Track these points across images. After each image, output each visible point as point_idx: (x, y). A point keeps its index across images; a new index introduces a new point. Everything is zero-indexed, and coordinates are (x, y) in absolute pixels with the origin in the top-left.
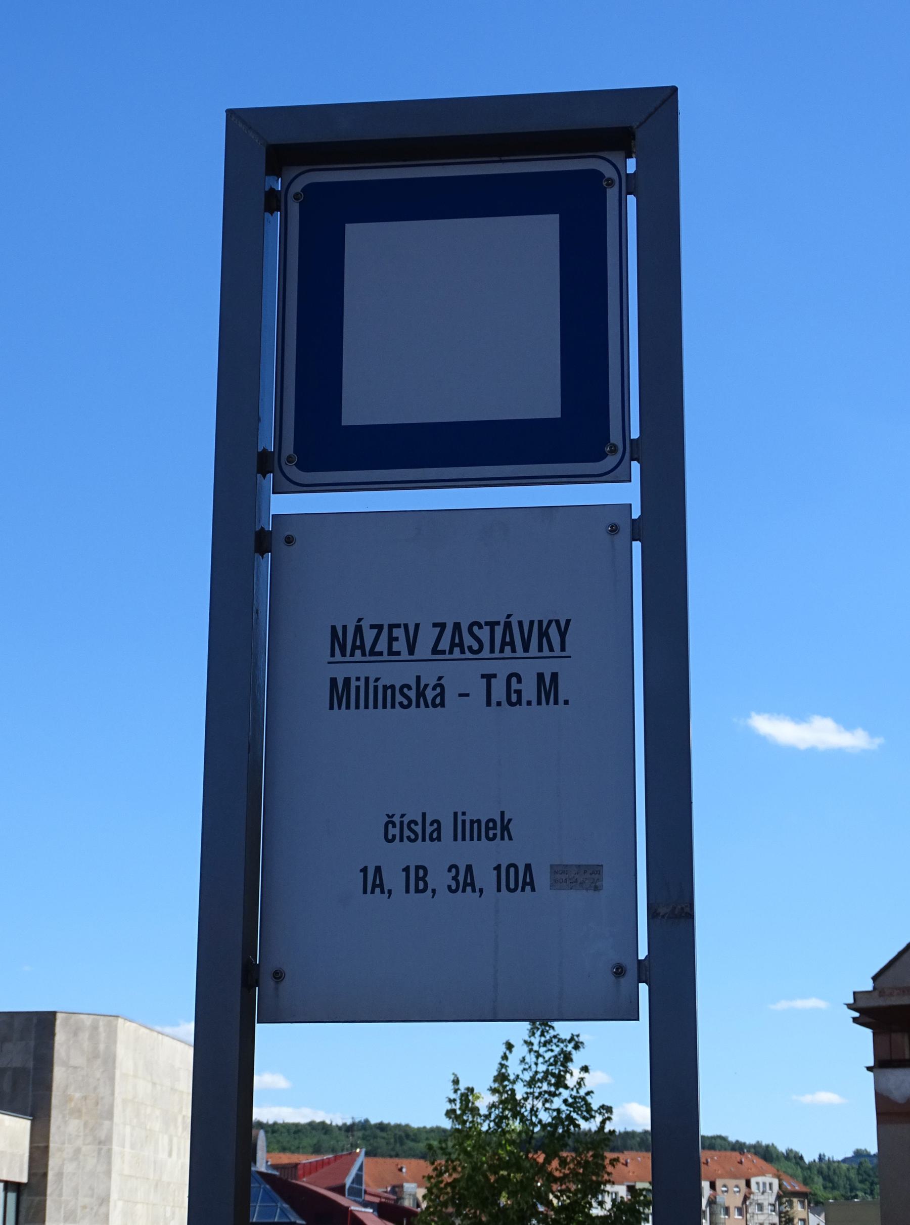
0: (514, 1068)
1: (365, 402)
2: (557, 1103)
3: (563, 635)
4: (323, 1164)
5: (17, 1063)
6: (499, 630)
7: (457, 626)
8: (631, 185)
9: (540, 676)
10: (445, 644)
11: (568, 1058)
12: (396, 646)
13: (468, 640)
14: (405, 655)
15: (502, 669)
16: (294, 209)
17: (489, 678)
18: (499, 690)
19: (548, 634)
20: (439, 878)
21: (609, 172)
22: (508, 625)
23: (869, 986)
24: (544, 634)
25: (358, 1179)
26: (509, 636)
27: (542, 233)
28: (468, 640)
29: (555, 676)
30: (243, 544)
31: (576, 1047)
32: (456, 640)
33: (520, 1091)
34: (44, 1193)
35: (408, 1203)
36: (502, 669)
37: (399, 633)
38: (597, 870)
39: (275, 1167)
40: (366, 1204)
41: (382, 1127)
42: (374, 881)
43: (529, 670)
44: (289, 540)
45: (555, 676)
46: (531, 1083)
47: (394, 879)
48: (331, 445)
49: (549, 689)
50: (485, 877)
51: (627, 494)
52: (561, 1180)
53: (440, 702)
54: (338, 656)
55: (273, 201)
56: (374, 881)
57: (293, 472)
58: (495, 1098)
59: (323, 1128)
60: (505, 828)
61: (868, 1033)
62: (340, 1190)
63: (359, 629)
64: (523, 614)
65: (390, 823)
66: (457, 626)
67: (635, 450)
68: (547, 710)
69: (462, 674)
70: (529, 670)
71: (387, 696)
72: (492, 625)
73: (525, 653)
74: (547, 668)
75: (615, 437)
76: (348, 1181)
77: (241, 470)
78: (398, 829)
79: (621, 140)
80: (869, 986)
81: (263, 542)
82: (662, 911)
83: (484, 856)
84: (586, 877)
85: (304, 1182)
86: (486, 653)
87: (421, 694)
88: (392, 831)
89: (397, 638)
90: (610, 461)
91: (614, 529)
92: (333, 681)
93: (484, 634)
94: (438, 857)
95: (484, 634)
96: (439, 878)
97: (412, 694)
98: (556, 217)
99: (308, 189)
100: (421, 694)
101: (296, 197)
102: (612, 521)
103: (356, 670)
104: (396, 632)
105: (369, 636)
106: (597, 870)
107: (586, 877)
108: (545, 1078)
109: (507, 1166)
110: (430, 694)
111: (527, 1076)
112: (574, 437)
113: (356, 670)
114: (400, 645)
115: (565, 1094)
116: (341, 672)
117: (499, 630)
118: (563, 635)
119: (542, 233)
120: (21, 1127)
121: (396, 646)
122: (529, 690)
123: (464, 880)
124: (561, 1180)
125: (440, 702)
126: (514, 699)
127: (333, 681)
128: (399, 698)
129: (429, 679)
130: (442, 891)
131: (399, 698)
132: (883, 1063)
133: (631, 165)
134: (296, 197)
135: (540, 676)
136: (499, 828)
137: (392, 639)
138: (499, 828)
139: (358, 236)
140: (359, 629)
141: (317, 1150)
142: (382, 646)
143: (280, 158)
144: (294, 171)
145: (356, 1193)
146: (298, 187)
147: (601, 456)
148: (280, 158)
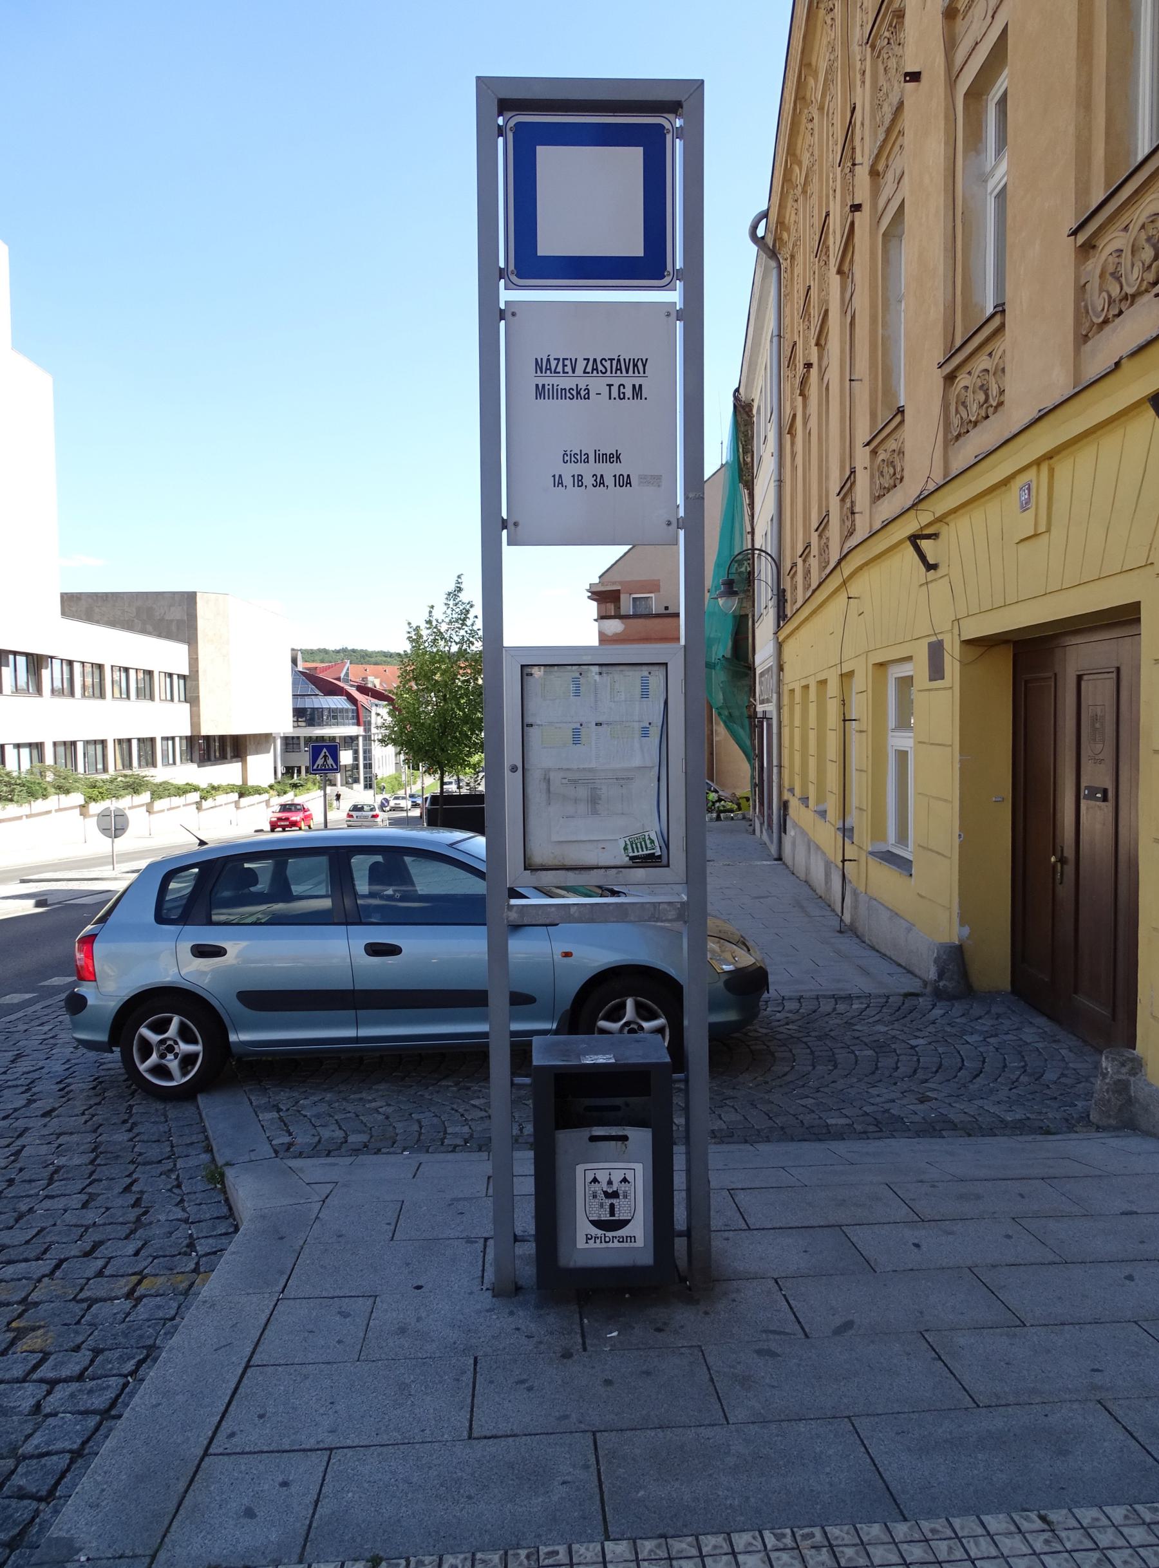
0: (438, 614)
1: (549, 245)
2: (462, 632)
3: (644, 366)
4: (329, 667)
5: (178, 618)
6: (614, 362)
7: (595, 360)
8: (679, 133)
9: (634, 386)
10: (589, 369)
11: (468, 611)
12: (566, 369)
13: (600, 368)
14: (570, 373)
15: (616, 382)
16: (510, 136)
17: (610, 386)
18: (615, 393)
19: (636, 365)
20: (588, 480)
21: (667, 125)
22: (619, 360)
23: (597, 581)
24: (635, 365)
25: (347, 674)
26: (621, 366)
27: (634, 156)
28: (600, 368)
29: (640, 386)
30: (491, 314)
31: (472, 606)
32: (595, 367)
33: (443, 627)
34: (197, 680)
35: (370, 685)
36: (616, 382)
37: (567, 362)
38: (659, 477)
39: (308, 669)
40: (352, 686)
41: (354, 651)
42: (559, 481)
43: (629, 382)
44: (514, 314)
45: (640, 386)
46: (451, 622)
47: (568, 481)
48: (531, 265)
49: (638, 392)
50: (609, 480)
51: (674, 297)
52: (465, 668)
53: (587, 397)
54: (539, 373)
55: (501, 131)
56: (559, 481)
57: (514, 278)
58: (429, 631)
59: (325, 651)
60: (618, 457)
61: (595, 604)
62: (339, 679)
63: (548, 360)
64: (626, 356)
65: (565, 454)
66: (595, 360)
67: (679, 275)
68: (637, 402)
69: (597, 384)
70: (629, 382)
71: (563, 394)
72: (612, 360)
73: (625, 372)
74: (637, 382)
75: (669, 267)
76: (342, 676)
77: (489, 278)
78: (570, 457)
79: (674, 107)
80: (597, 581)
81: (502, 315)
82: (691, 495)
83: (608, 470)
84: (654, 480)
85: (321, 676)
86: (608, 373)
87: (578, 393)
88: (567, 458)
89: (568, 365)
90: (667, 280)
91: (668, 315)
92: (537, 386)
93: (607, 364)
94: (587, 470)
95: (607, 364)
96: (588, 480)
97: (574, 393)
98: (641, 149)
99: (518, 124)
100: (578, 393)
101: (511, 129)
102: (667, 310)
103: (548, 380)
104: (567, 362)
105: (553, 363)
106: (659, 477)
107: (654, 480)
108: (457, 621)
109: (439, 662)
110: (583, 393)
111: (447, 620)
112: (648, 266)
113: (548, 380)
114: (568, 369)
115: (466, 629)
116: (540, 383)
117: (614, 362)
118: (644, 366)
119: (634, 156)
120: (183, 648)
121: (566, 369)
122: (629, 392)
123: (600, 481)
124: (465, 668)
125: (587, 397)
126: (621, 396)
127: (537, 386)
128: (568, 395)
129: (582, 386)
130: (590, 487)
131: (568, 395)
132: (602, 617)
133: (678, 123)
134: (511, 129)
135: (634, 386)
136: (616, 457)
137: (564, 366)
138: (616, 457)
139: (542, 151)
140: (548, 360)
141: (322, 662)
142: (560, 369)
143: (505, 106)
144: (510, 114)
145: (346, 681)
146: (512, 123)
147: (663, 277)
148: (505, 106)
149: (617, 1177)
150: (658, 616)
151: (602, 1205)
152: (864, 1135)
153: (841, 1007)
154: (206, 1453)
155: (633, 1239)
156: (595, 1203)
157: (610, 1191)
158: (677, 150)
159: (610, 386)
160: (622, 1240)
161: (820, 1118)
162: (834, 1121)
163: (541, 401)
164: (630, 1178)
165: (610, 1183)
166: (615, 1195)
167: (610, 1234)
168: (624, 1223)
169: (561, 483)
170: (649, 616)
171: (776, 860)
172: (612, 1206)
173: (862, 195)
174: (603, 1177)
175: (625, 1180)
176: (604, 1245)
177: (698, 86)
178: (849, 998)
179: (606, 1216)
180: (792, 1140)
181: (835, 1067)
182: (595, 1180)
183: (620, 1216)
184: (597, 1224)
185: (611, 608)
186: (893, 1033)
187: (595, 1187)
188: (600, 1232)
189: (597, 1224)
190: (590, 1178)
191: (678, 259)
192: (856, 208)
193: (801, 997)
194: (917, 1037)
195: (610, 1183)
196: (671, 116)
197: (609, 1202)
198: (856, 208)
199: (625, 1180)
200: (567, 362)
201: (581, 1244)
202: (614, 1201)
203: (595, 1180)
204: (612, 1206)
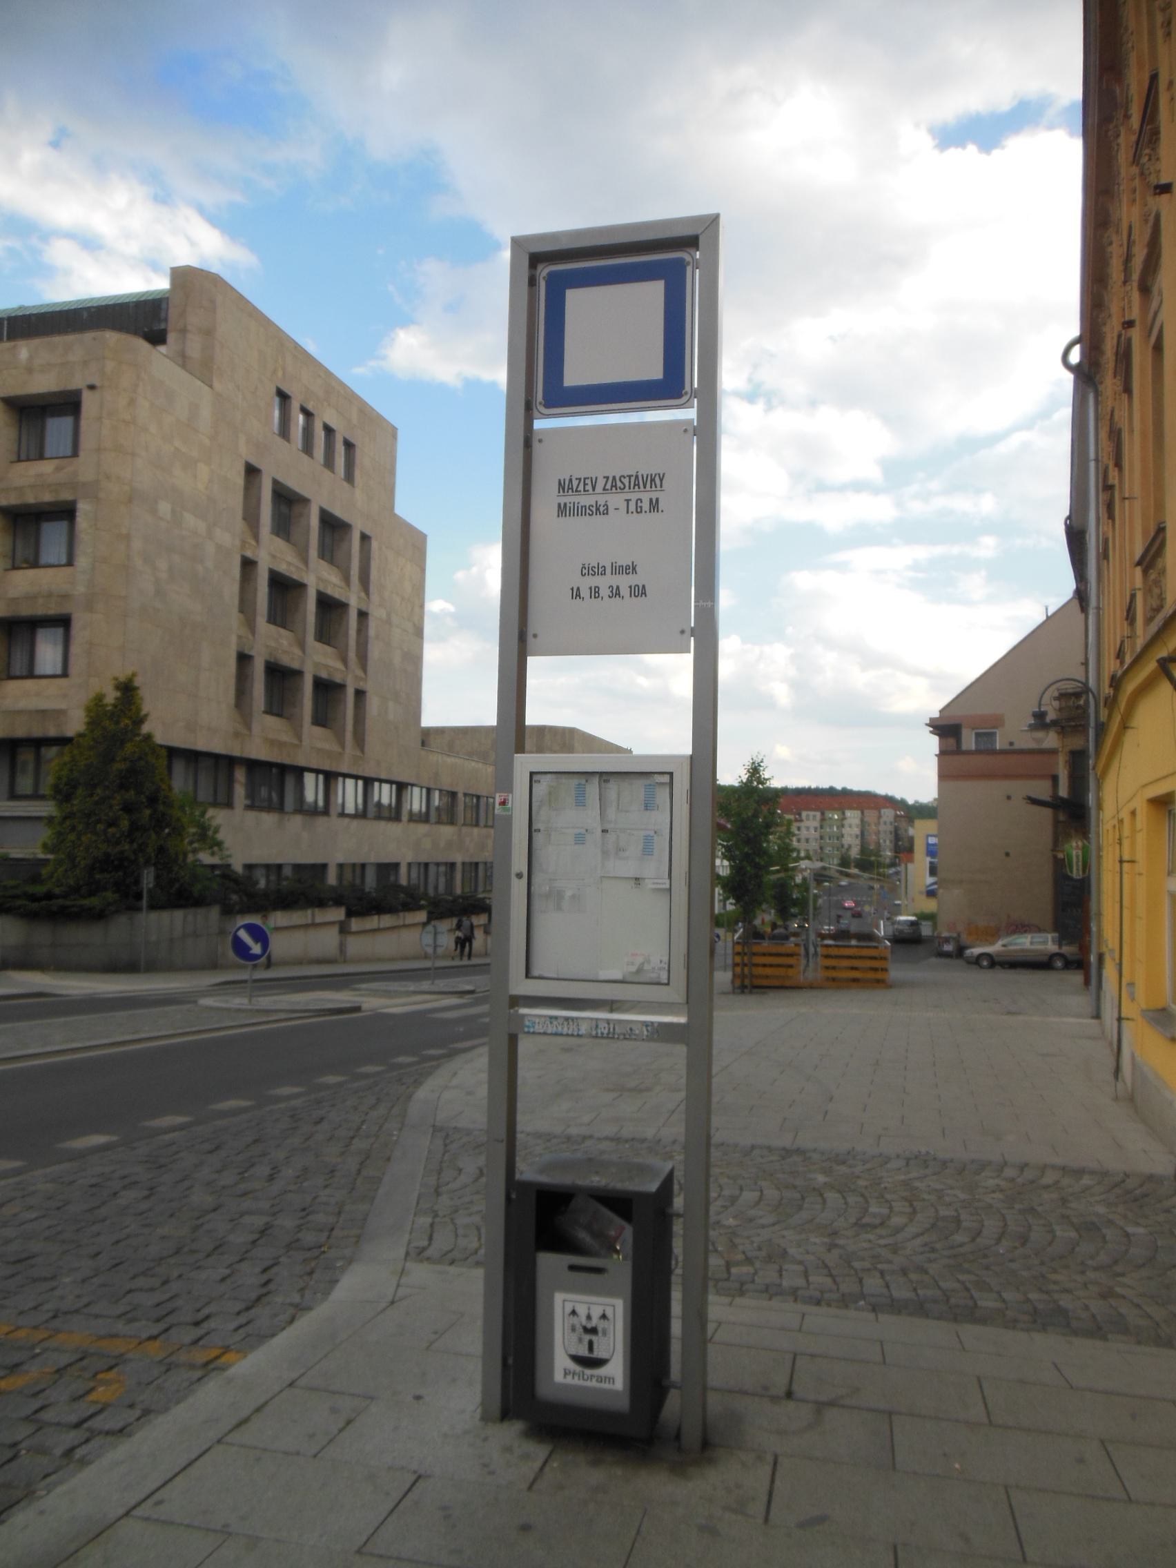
3: (661, 480)
7: (614, 478)
9: (651, 500)
10: (608, 487)
13: (619, 484)
17: (628, 501)
18: (632, 507)
19: (655, 481)
20: (605, 592)
22: (637, 477)
23: (937, 715)
24: (653, 480)
26: (638, 482)
28: (619, 484)
32: (614, 484)
36: (633, 497)
37: (588, 481)
42: (576, 594)
43: (646, 497)
45: (657, 500)
47: (585, 593)
49: (654, 505)
50: (625, 591)
51: (690, 414)
53: (606, 512)
56: (576, 594)
60: (634, 569)
63: (571, 480)
64: (644, 471)
66: (614, 478)
67: (695, 394)
68: (654, 515)
69: (616, 500)
70: (646, 497)
71: (583, 511)
72: (630, 477)
73: (643, 490)
74: (654, 496)
78: (587, 571)
83: (624, 582)
87: (598, 509)
89: (588, 484)
90: (685, 399)
93: (626, 481)
95: (626, 481)
96: (605, 592)
99: (551, 274)
100: (598, 509)
103: (570, 499)
105: (575, 483)
110: (602, 509)
112: (669, 387)
113: (570, 499)
114: (589, 487)
117: (633, 479)
118: (661, 480)
122: (646, 506)
123: (616, 593)
125: (606, 512)
126: (639, 510)
127: (559, 505)
129: (601, 502)
130: (606, 598)
137: (585, 484)
138: (632, 569)
140: (571, 480)
142: (581, 488)
147: (680, 396)
148: (536, 260)
149: (596, 1312)
150: (1003, 752)
151: (580, 1340)
152: (1012, 1324)
153: (1066, 1181)
154: (127, 1514)
155: (611, 1380)
156: (574, 1337)
157: (589, 1326)
158: (695, 280)
159: (628, 501)
160: (600, 1379)
161: (972, 1297)
162: (987, 1302)
163: (562, 519)
164: (609, 1313)
165: (589, 1317)
166: (594, 1331)
167: (588, 1372)
168: (598, 1363)
169: (578, 595)
170: (994, 752)
171: (1093, 1018)
172: (591, 1344)
173: (1135, 314)
174: (582, 1311)
175: (604, 1317)
176: (581, 1383)
177: (713, 222)
178: (1079, 1173)
179: (583, 1351)
180: (927, 1316)
181: (1023, 1245)
182: (574, 1313)
183: (599, 1353)
184: (577, 1359)
185: (951, 742)
186: (1111, 1217)
187: (574, 1320)
188: (578, 1368)
189: (577, 1359)
190: (568, 1309)
191: (694, 378)
192: (1129, 324)
193: (1026, 1165)
194: (1138, 1224)
195: (589, 1317)
196: (692, 251)
197: (587, 1338)
198: (1129, 324)
199: (604, 1317)
200: (588, 481)
201: (559, 1377)
202: (594, 1338)
203: (574, 1313)
204: (591, 1344)
